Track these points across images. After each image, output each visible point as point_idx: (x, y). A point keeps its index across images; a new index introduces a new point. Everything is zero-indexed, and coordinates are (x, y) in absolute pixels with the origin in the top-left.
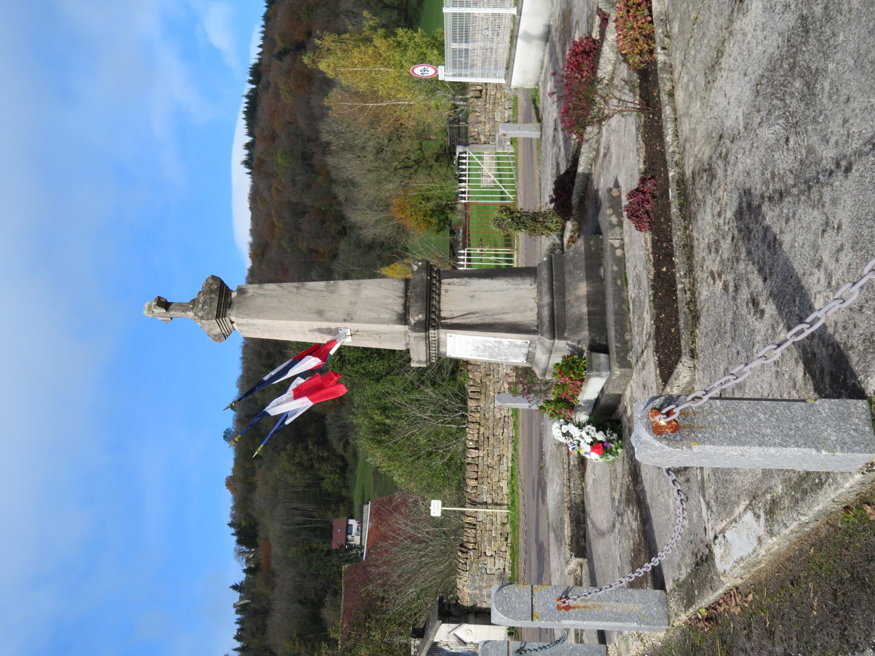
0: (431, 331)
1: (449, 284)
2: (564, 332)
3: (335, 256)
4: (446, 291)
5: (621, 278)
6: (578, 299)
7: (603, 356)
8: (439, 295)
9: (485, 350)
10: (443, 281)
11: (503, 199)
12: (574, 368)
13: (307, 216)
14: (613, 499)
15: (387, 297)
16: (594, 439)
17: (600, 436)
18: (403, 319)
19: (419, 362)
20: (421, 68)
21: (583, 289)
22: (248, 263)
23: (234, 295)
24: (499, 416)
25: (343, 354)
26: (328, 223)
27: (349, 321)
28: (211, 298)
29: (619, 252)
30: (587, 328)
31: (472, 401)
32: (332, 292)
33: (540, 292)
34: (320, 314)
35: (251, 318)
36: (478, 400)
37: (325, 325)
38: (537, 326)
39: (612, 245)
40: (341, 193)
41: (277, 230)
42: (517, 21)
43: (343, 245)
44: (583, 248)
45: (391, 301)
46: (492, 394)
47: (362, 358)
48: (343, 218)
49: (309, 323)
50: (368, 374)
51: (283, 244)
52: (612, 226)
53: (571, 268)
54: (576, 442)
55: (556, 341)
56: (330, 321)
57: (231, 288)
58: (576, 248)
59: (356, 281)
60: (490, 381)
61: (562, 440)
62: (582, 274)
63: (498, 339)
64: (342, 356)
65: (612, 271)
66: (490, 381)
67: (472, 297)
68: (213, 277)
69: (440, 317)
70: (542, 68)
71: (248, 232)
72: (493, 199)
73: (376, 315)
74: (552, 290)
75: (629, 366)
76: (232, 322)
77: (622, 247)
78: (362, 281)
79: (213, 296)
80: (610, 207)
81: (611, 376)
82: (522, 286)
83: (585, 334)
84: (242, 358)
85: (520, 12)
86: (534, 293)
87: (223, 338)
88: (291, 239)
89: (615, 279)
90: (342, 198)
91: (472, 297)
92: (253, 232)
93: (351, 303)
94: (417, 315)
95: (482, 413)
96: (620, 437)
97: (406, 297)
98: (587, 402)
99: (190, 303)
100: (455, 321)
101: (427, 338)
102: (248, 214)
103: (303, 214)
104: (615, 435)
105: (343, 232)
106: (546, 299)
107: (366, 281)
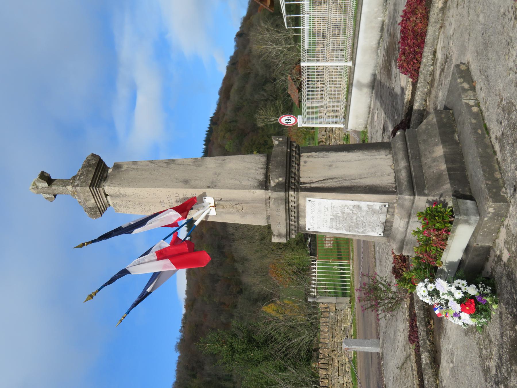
0: (291, 193)
1: (308, 157)
2: (423, 189)
3: (235, 307)
4: (305, 162)
5: (480, 128)
6: (435, 160)
7: (469, 203)
8: (299, 165)
9: (344, 219)
10: (302, 155)
11: (335, 289)
12: (439, 222)
13: (220, 282)
14: (486, 371)
15: (249, 169)
16: (465, 293)
17: (472, 290)
18: (264, 185)
19: (280, 236)
20: (286, 118)
21: (439, 151)
22: (184, 311)
23: (110, 171)
24: (342, 382)
25: (234, 346)
26: (232, 286)
27: (212, 187)
28: (88, 171)
29: (475, 109)
30: (448, 181)
31: (322, 370)
33: (395, 161)
34: (186, 183)
35: (122, 186)
36: (327, 369)
38: (396, 188)
39: (467, 104)
40: (239, 267)
41: (201, 291)
42: (352, 70)
43: (240, 299)
44: (435, 120)
45: (253, 171)
46: (337, 365)
47: (246, 349)
48: (241, 283)
49: (175, 190)
50: (251, 361)
51: (205, 299)
52: (465, 90)
53: (425, 138)
54: (443, 302)
55: (417, 197)
56: (195, 187)
57: (108, 165)
58: (427, 122)
60: (335, 355)
61: (428, 300)
62: (437, 139)
63: (356, 203)
64: (233, 348)
65: (471, 123)
66: (335, 355)
67: (330, 166)
68: (93, 155)
69: (299, 182)
70: (369, 113)
71: (185, 292)
72: (331, 289)
73: (238, 183)
74: (408, 157)
75: (504, 200)
76: (106, 195)
77: (478, 105)
78: (227, 157)
79: (90, 169)
80: (460, 77)
81: (481, 219)
82: (377, 157)
83: (447, 186)
84: (177, 370)
85: (354, 64)
86: (390, 162)
87: (98, 213)
89: (475, 129)
90: (240, 271)
91: (330, 166)
92: (187, 292)
93: (216, 173)
94: (278, 178)
95: (330, 379)
96: (494, 292)
97: (267, 169)
98: (451, 265)
99: (71, 179)
100: (313, 185)
101: (287, 201)
102: (186, 281)
103: (217, 281)
104: (488, 290)
105: (241, 292)
106: (403, 164)
107: (230, 157)
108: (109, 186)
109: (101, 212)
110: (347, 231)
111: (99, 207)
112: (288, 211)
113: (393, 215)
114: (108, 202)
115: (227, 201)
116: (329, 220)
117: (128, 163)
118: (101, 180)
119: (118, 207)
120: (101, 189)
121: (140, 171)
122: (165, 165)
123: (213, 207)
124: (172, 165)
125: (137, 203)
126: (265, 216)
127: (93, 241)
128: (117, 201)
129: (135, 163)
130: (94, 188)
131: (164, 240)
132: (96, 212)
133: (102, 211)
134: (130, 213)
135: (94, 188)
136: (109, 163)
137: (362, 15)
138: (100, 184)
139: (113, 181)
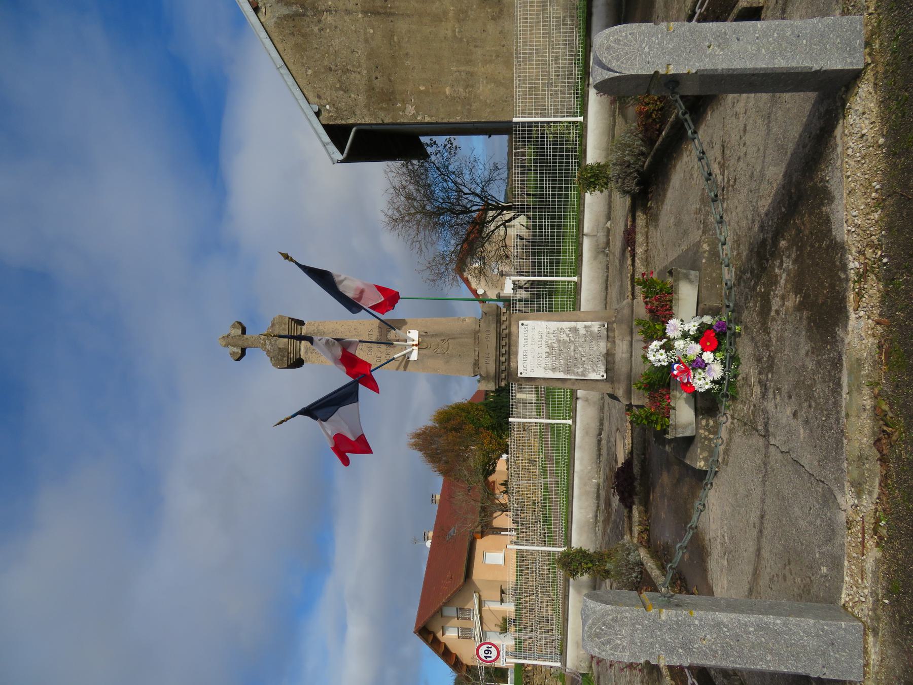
110: (564, 372)
112: (499, 337)
113: (614, 342)
116: (544, 355)
126: (471, 360)
127: (297, 263)
137: (575, 474)
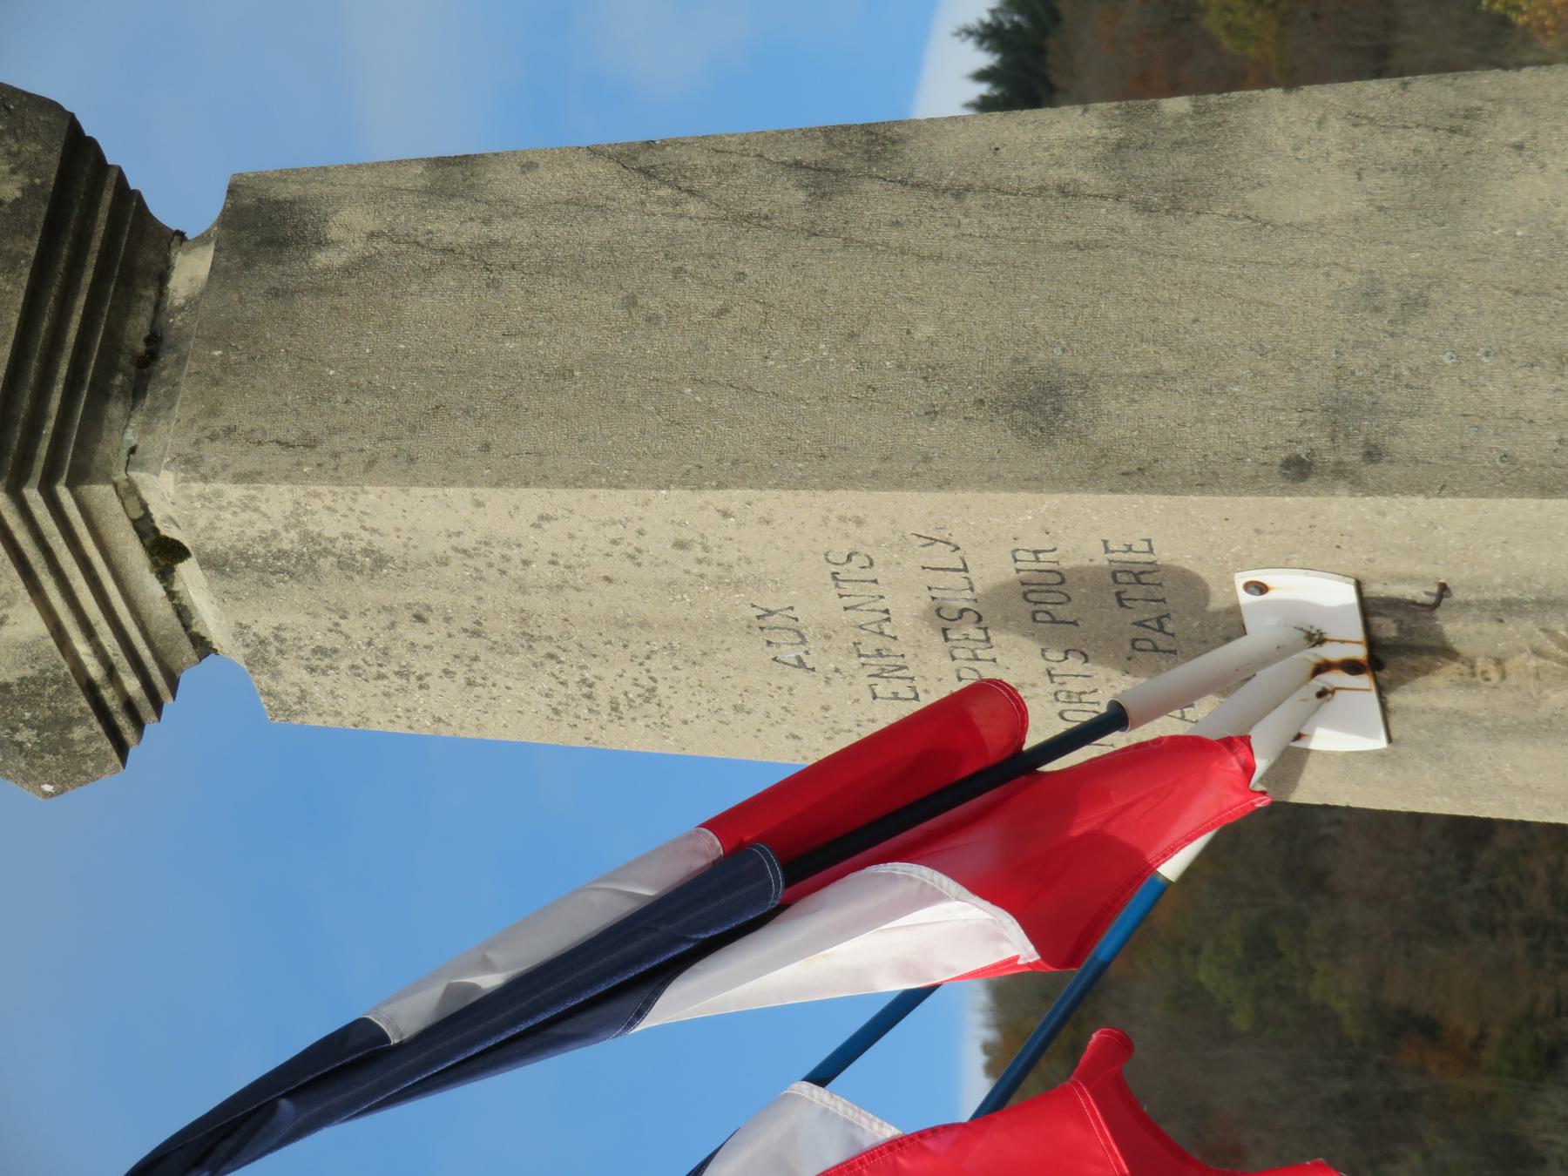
23: (190, 272)
32: (1177, 200)
34: (1041, 417)
35: (334, 471)
37: (1090, 527)
49: (918, 508)
51: (1207, 974)
56: (1139, 475)
57: (165, 209)
59: (1430, 93)
76: (166, 554)
78: (1488, 82)
87: (88, 732)
88: (1260, 947)
93: (1370, 296)
108: (190, 464)
109: (119, 726)
111: (95, 670)
114: (183, 613)
115: (1507, 608)
117: (381, 183)
118: (101, 393)
119: (293, 674)
120: (101, 494)
121: (511, 280)
122: (791, 197)
123: (1352, 667)
124: (876, 203)
125: (503, 628)
128: (284, 612)
129: (453, 175)
130: (32, 495)
131: (822, 1076)
132: (70, 723)
133: (129, 706)
134: (425, 726)
135: (32, 495)
136: (181, 191)
138: (85, 446)
139: (234, 412)
